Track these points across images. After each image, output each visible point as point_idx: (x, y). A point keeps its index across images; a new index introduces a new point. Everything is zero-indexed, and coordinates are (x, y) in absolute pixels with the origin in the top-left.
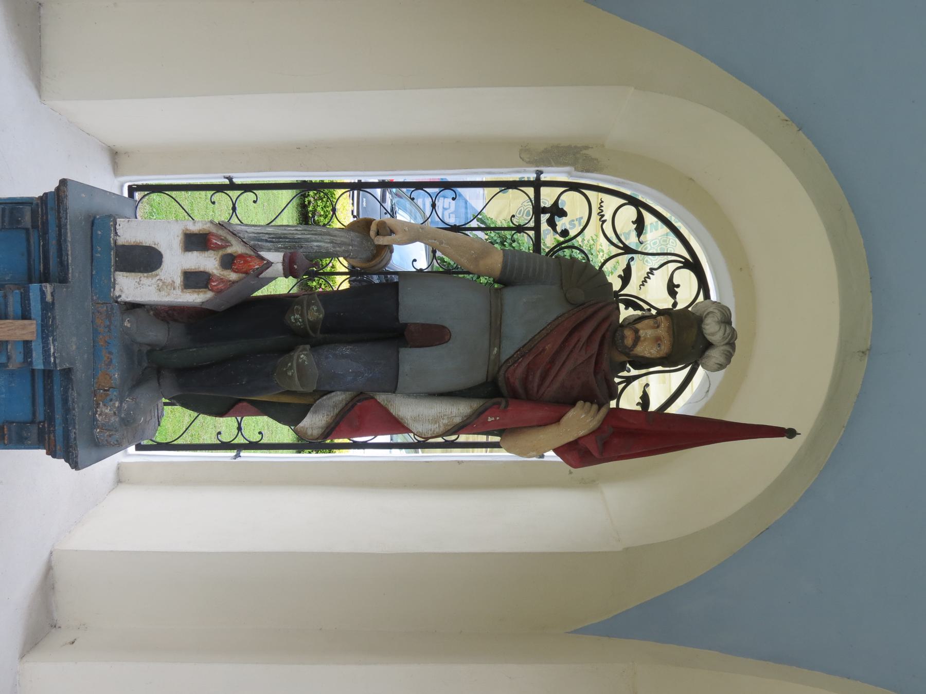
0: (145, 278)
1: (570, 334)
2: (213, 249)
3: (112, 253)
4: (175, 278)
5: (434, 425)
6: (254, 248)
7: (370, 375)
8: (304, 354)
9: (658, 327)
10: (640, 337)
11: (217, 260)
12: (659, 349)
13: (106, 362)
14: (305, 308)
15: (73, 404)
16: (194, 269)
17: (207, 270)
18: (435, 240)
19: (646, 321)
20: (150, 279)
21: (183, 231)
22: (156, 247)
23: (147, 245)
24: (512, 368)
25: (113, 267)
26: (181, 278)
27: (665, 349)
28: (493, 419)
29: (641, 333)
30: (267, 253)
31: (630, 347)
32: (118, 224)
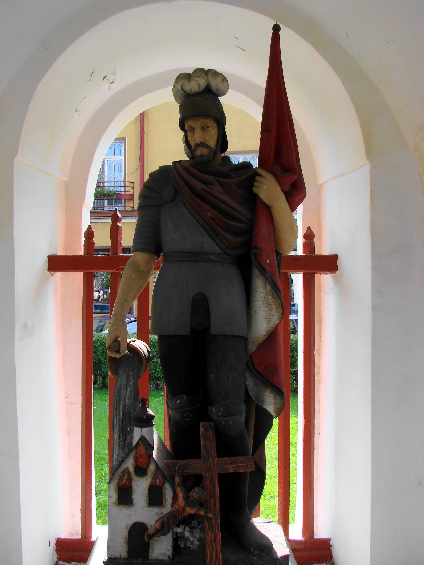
5: (272, 306)
6: (130, 451)
7: (232, 357)
9: (193, 129)
10: (201, 143)
12: (210, 128)
19: (189, 138)
22: (129, 527)
23: (127, 534)
29: (198, 141)
30: (134, 439)
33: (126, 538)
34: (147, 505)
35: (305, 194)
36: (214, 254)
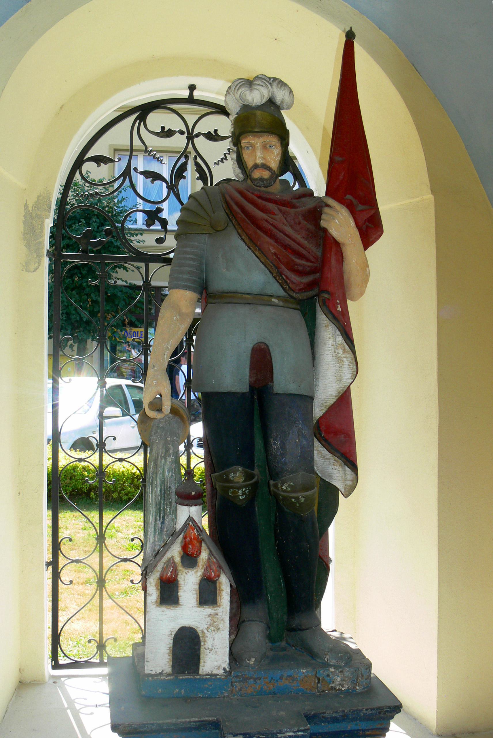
0: (206, 643)
1: (261, 228)
2: (176, 576)
3: (181, 677)
4: (205, 614)
5: (344, 362)
6: (174, 534)
7: (301, 422)
8: (282, 486)
11: (188, 572)
13: (291, 681)
14: (231, 485)
15: (339, 713)
16: (197, 595)
17: (198, 582)
18: (165, 355)
20: (207, 638)
21: (157, 606)
22: (174, 633)
23: (172, 642)
24: (291, 285)
25: (195, 677)
26: (206, 608)
27: (274, 140)
28: (339, 306)
29: (259, 161)
31: (271, 174)
32: (150, 672)
33: (170, 647)
34: (197, 604)
35: (382, 232)
36: (278, 297)
